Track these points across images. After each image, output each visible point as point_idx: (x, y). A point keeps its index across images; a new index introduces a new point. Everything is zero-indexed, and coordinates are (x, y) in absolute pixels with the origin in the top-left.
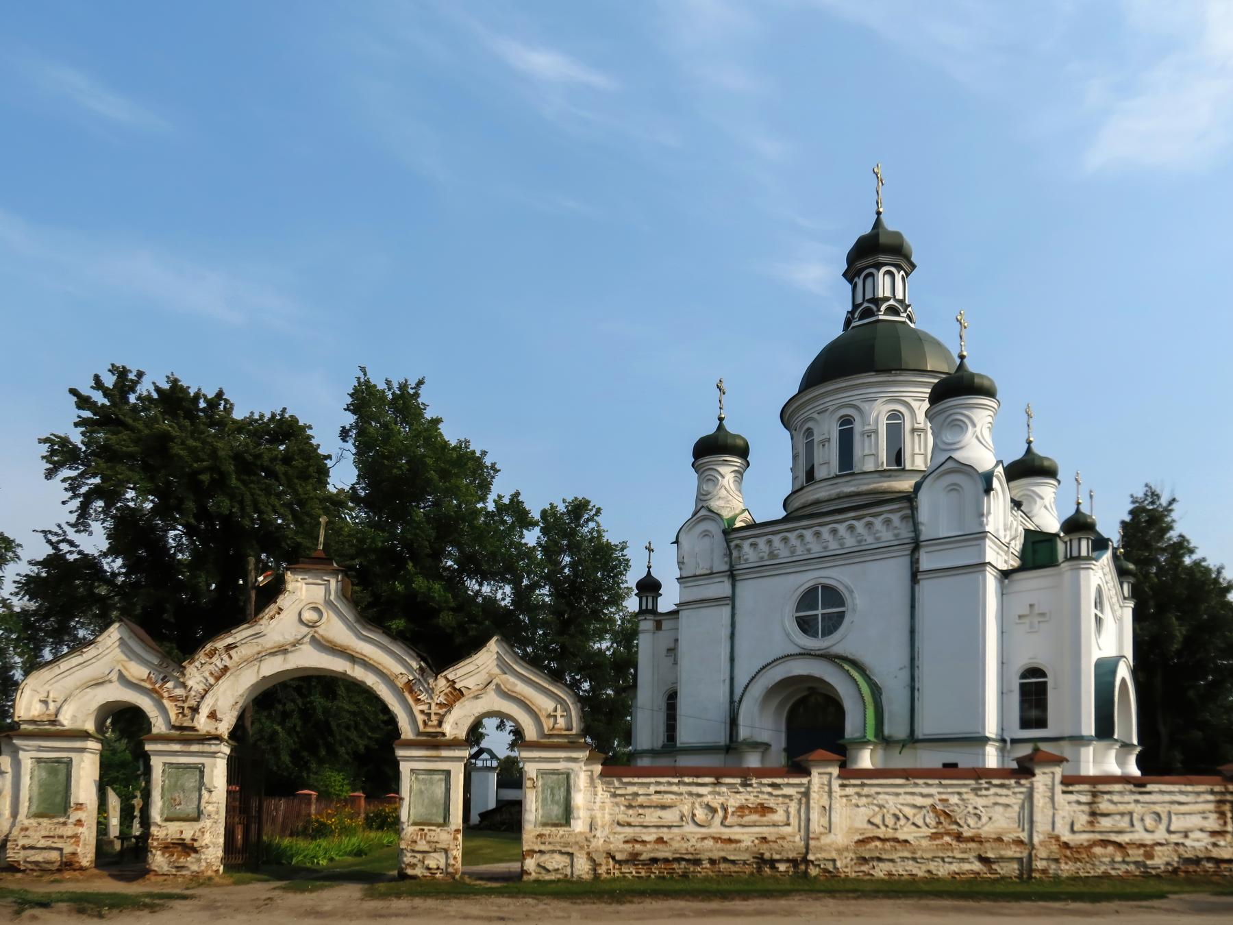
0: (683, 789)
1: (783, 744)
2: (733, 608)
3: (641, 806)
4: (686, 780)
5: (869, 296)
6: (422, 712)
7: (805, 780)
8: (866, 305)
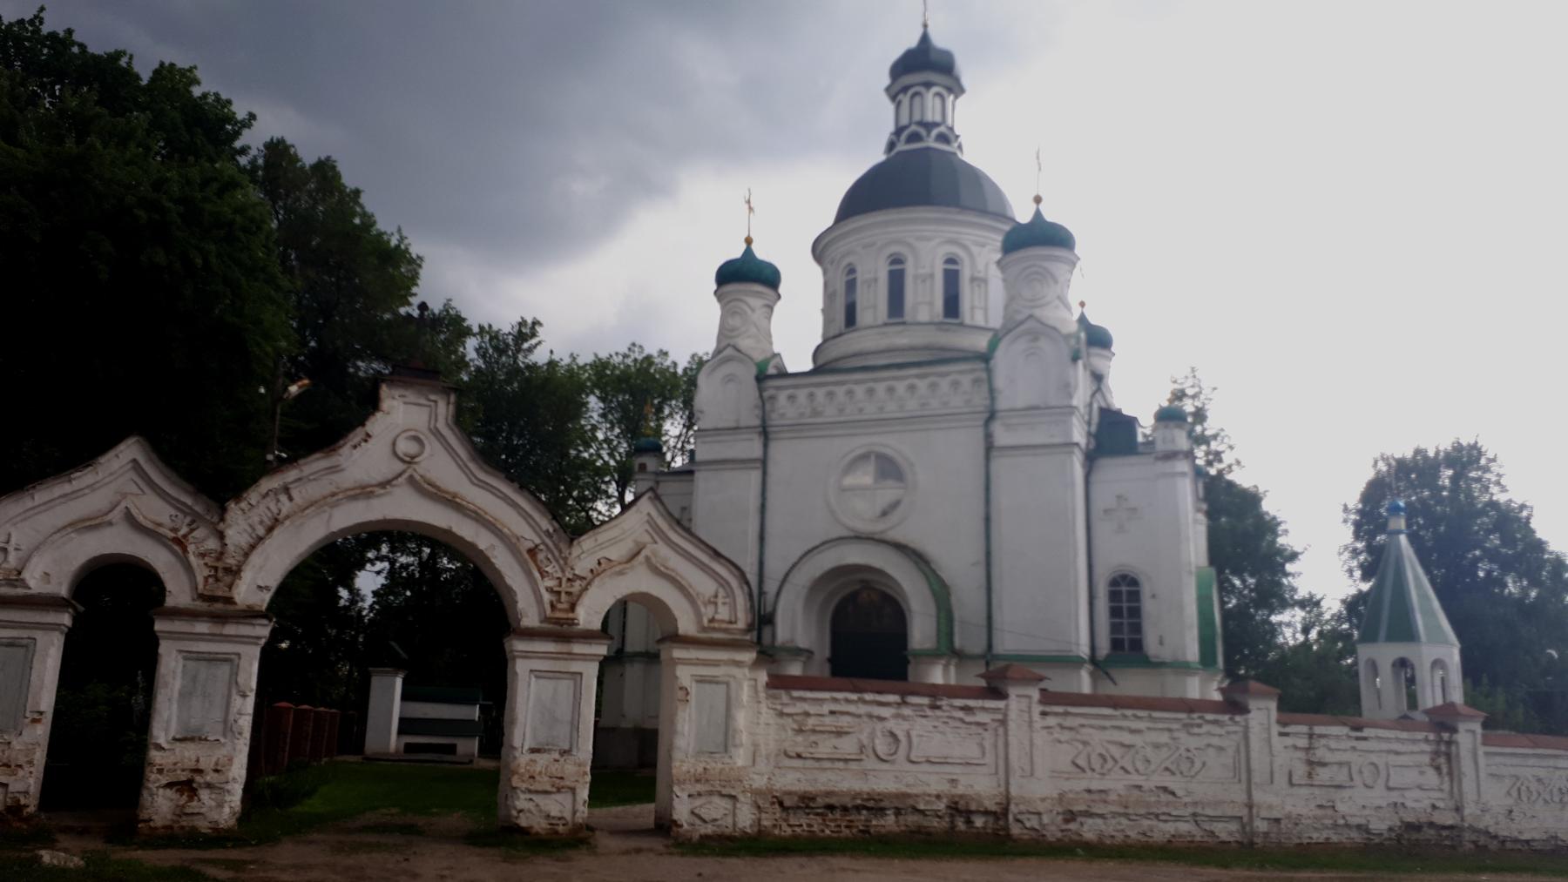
0: (862, 709)
1: (827, 653)
2: (765, 473)
3: (814, 731)
4: (868, 697)
5: (917, 117)
6: (550, 590)
7: (1000, 704)
8: (914, 128)
